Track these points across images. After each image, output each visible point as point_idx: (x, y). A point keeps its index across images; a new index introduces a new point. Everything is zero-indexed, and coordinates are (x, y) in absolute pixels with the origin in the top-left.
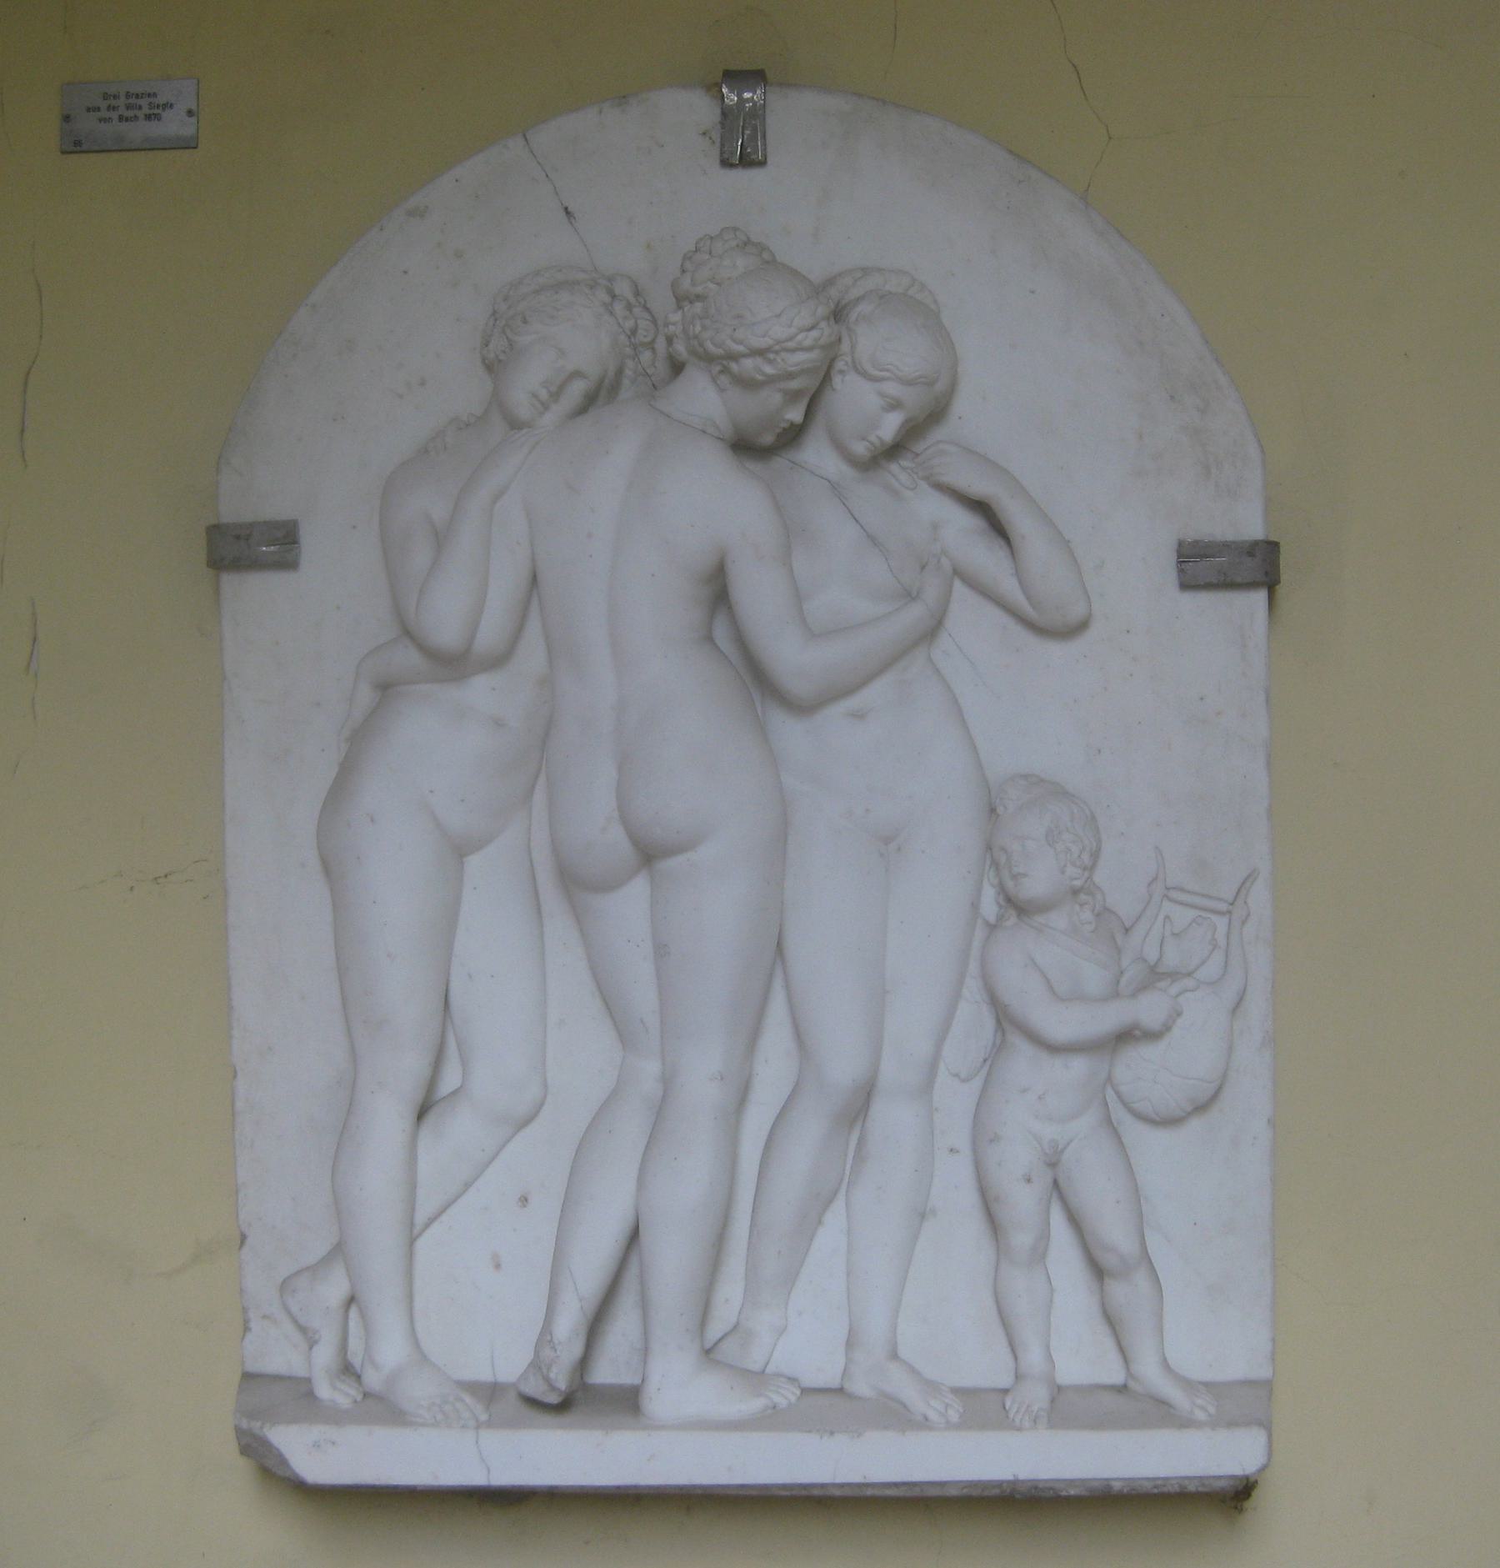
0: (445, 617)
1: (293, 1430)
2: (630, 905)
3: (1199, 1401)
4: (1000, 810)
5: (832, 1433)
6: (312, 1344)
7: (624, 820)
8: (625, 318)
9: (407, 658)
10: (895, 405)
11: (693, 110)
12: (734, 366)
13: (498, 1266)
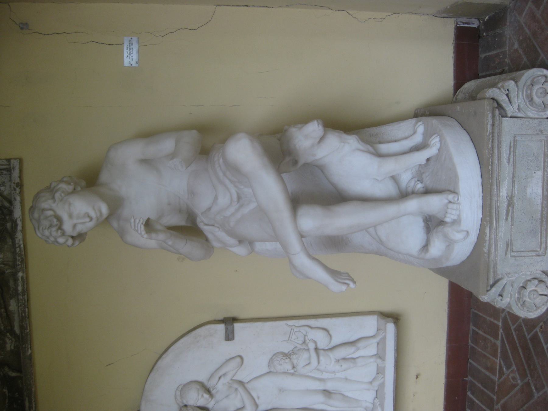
10: (203, 396)
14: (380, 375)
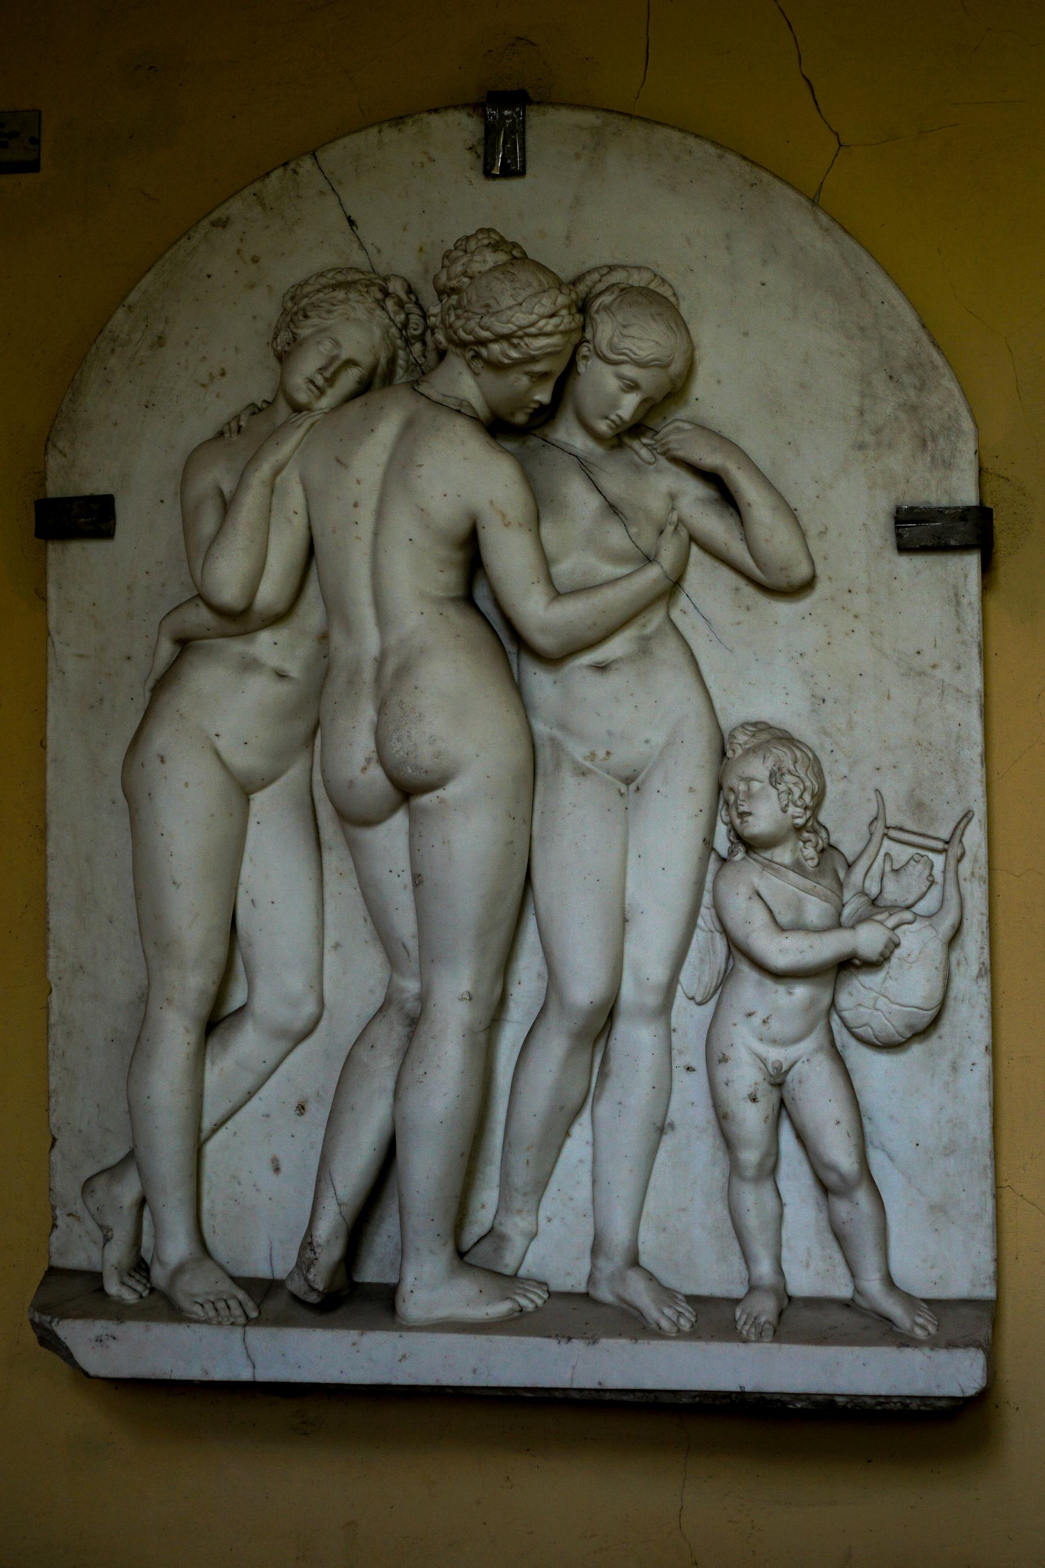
0: (227, 577)
1: (78, 1324)
2: (390, 838)
3: (920, 1320)
4: (730, 754)
5: (570, 1339)
6: (107, 1240)
7: (382, 761)
8: (396, 313)
9: (200, 617)
10: (633, 386)
11: (460, 129)
12: (484, 352)
13: (277, 1170)
14: (688, 1312)
